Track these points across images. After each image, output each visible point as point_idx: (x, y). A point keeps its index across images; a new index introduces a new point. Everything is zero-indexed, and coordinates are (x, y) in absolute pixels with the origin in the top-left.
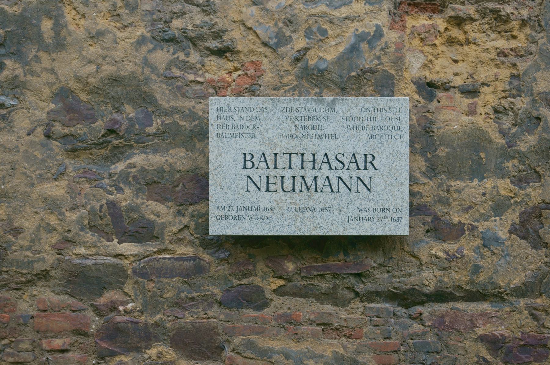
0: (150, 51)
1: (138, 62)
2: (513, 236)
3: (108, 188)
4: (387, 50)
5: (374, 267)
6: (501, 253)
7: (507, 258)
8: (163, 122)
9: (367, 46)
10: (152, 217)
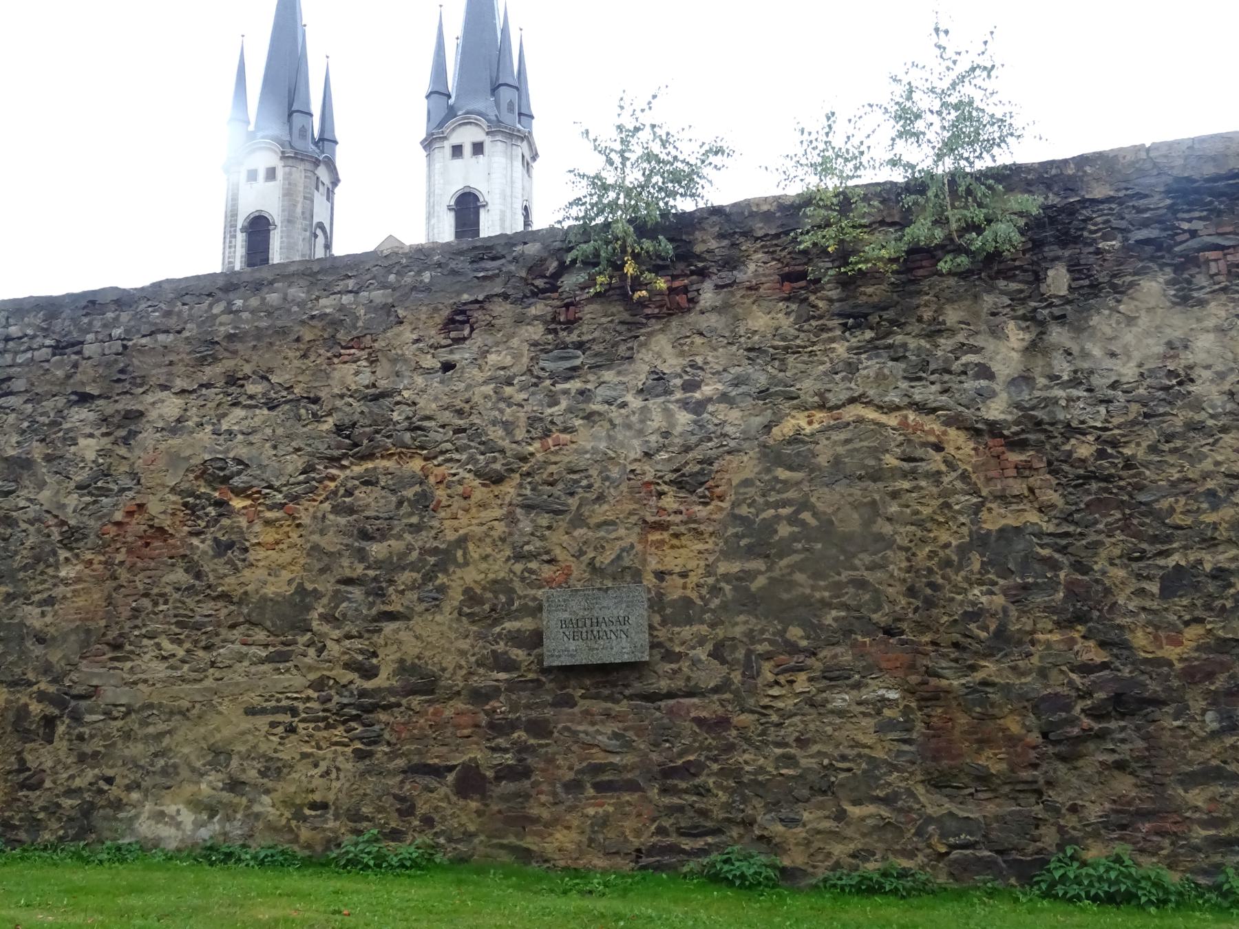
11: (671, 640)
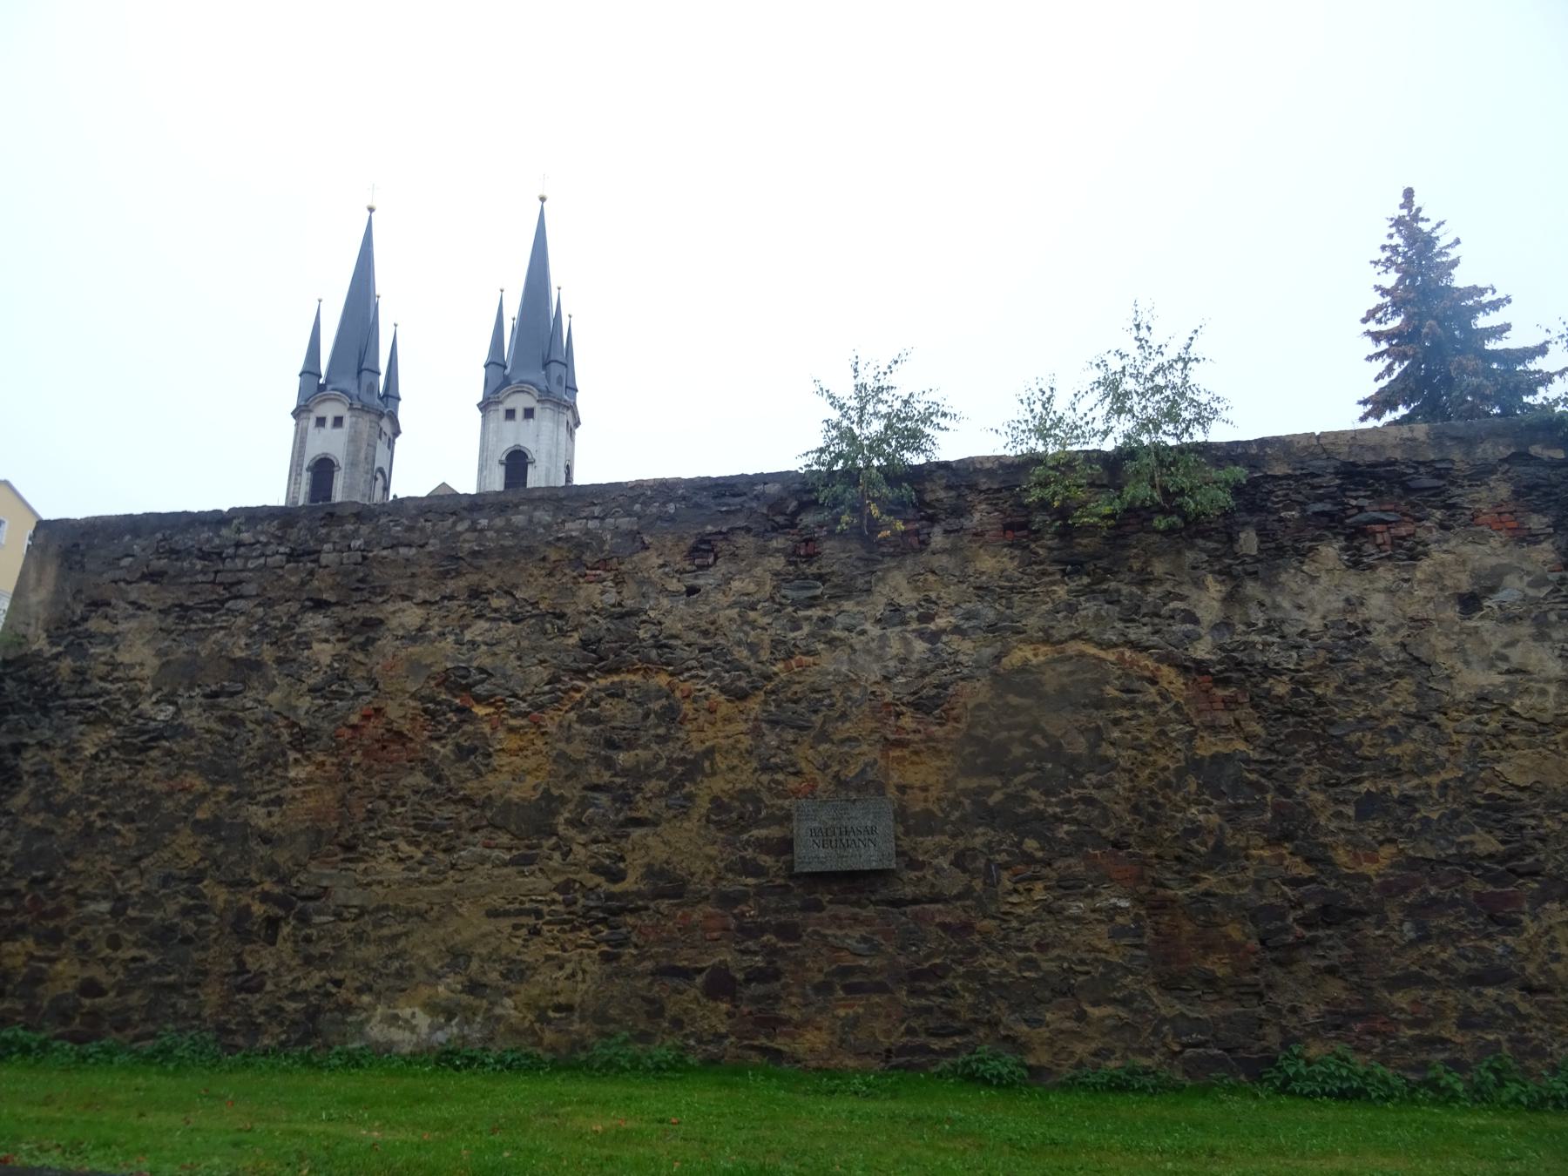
11: (914, 849)
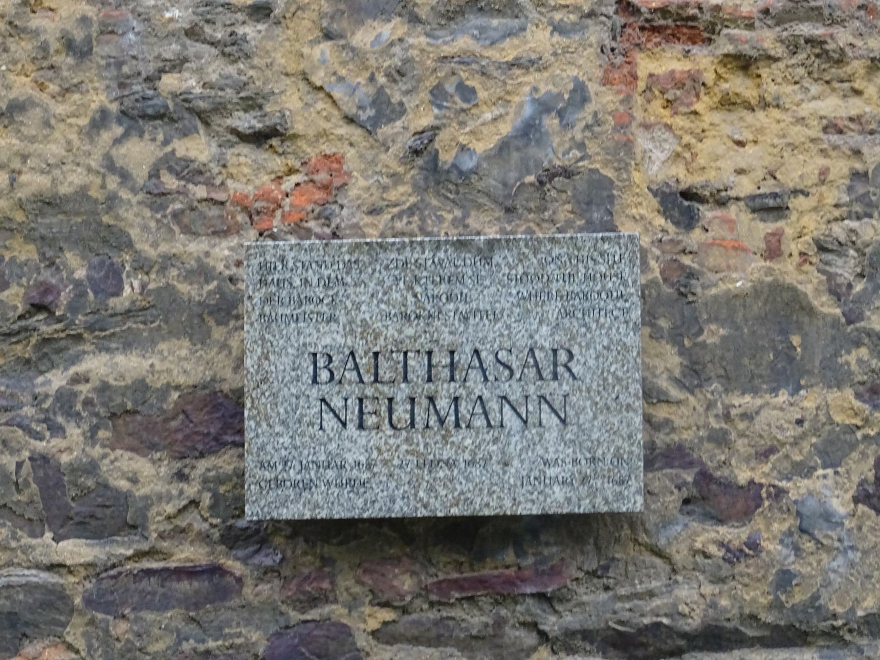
0: (118, 141)
1: (93, 164)
2: (861, 507)
3: (34, 426)
4: (597, 129)
5: (577, 579)
6: (837, 544)
7: (850, 554)
8: (143, 286)
9: (556, 121)
10: (123, 485)
11: (720, 439)
